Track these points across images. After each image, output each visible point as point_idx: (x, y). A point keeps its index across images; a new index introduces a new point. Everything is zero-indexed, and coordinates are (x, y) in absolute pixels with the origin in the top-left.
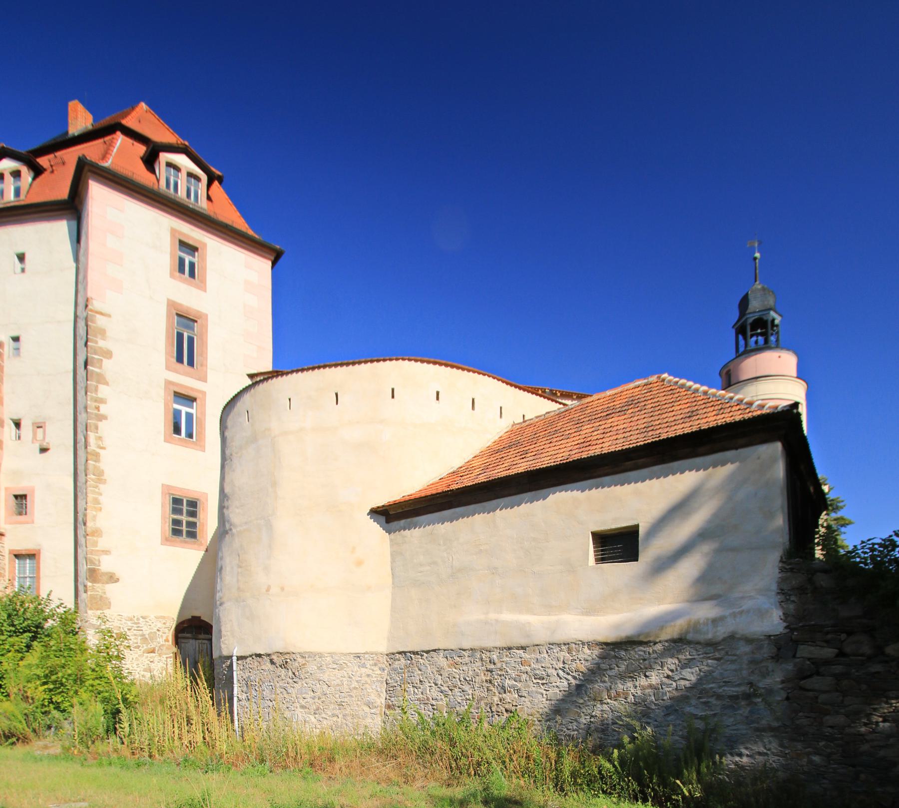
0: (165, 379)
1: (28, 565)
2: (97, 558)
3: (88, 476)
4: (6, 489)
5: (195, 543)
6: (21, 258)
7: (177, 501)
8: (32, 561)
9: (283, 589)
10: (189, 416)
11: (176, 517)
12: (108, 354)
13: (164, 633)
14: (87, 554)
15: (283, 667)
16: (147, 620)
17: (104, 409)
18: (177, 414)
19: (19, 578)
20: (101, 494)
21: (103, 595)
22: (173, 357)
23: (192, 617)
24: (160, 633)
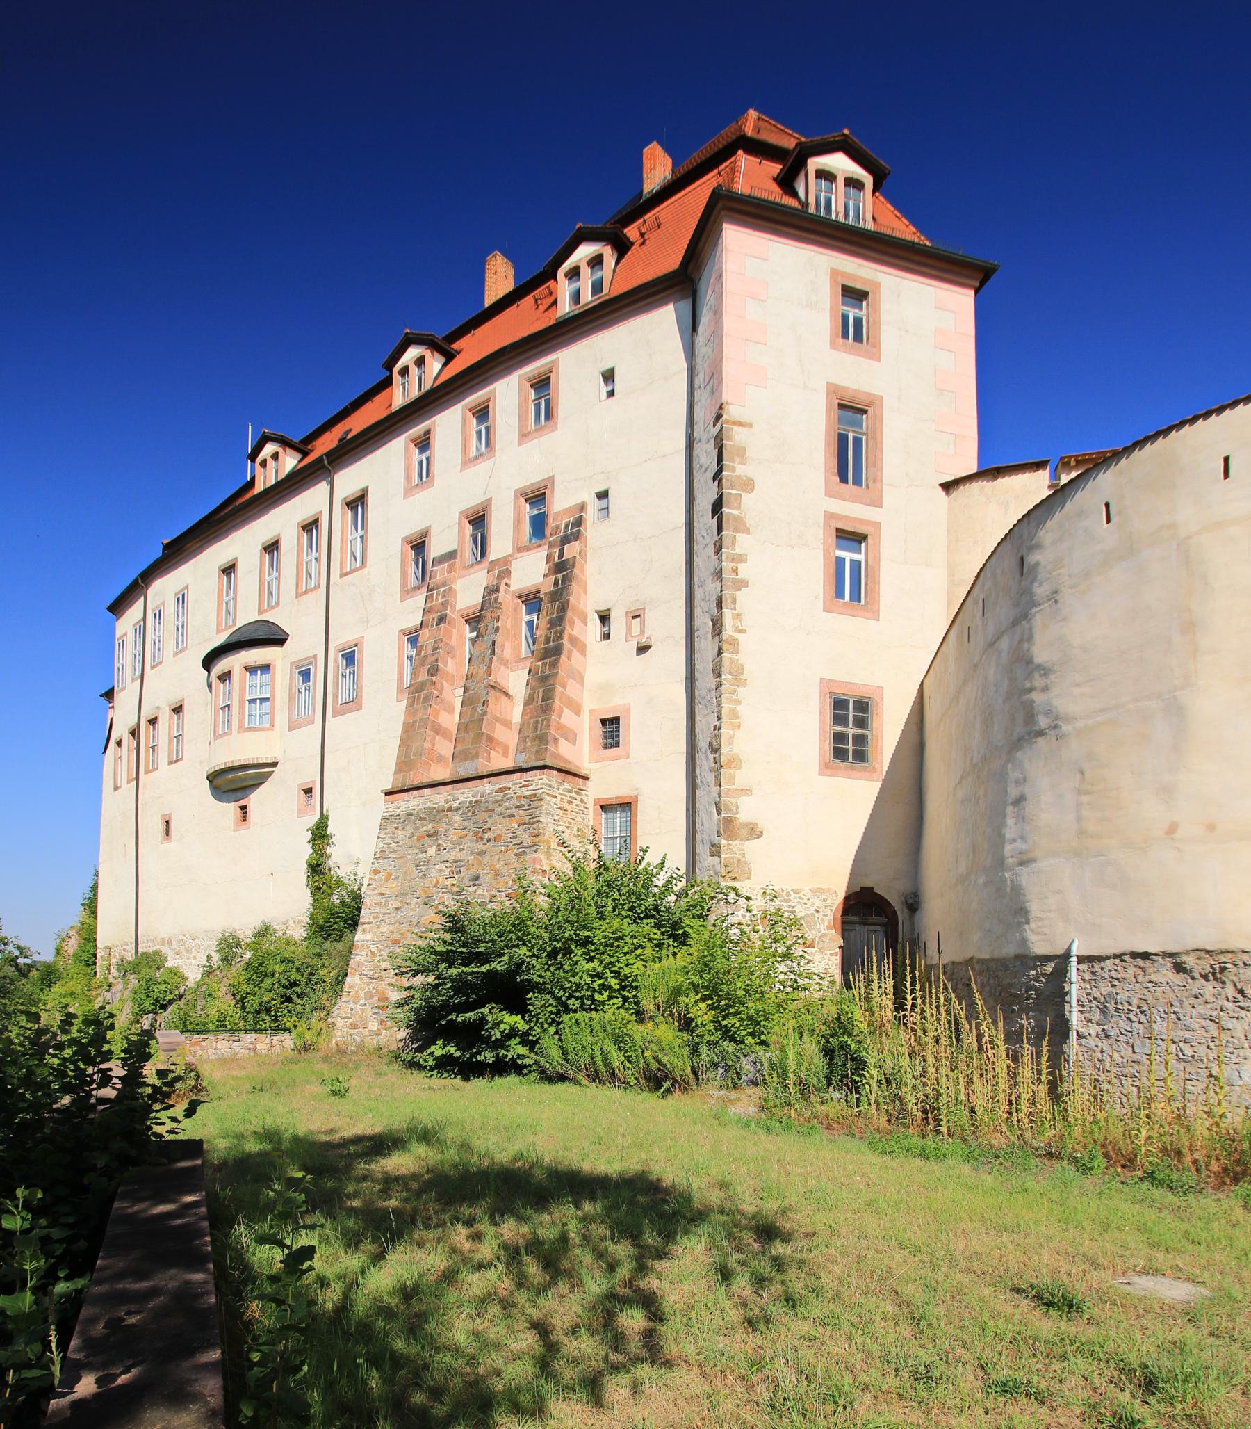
1: (618, 820)
2: (733, 801)
3: (723, 677)
4: (591, 711)
5: (865, 769)
6: (609, 376)
7: (840, 704)
8: (624, 814)
9: (1211, 828)
10: (856, 565)
11: (838, 729)
12: (749, 485)
14: (720, 796)
15: (1211, 977)
16: (801, 895)
17: (744, 571)
19: (607, 838)
20: (739, 703)
21: (741, 857)
24: (820, 915)
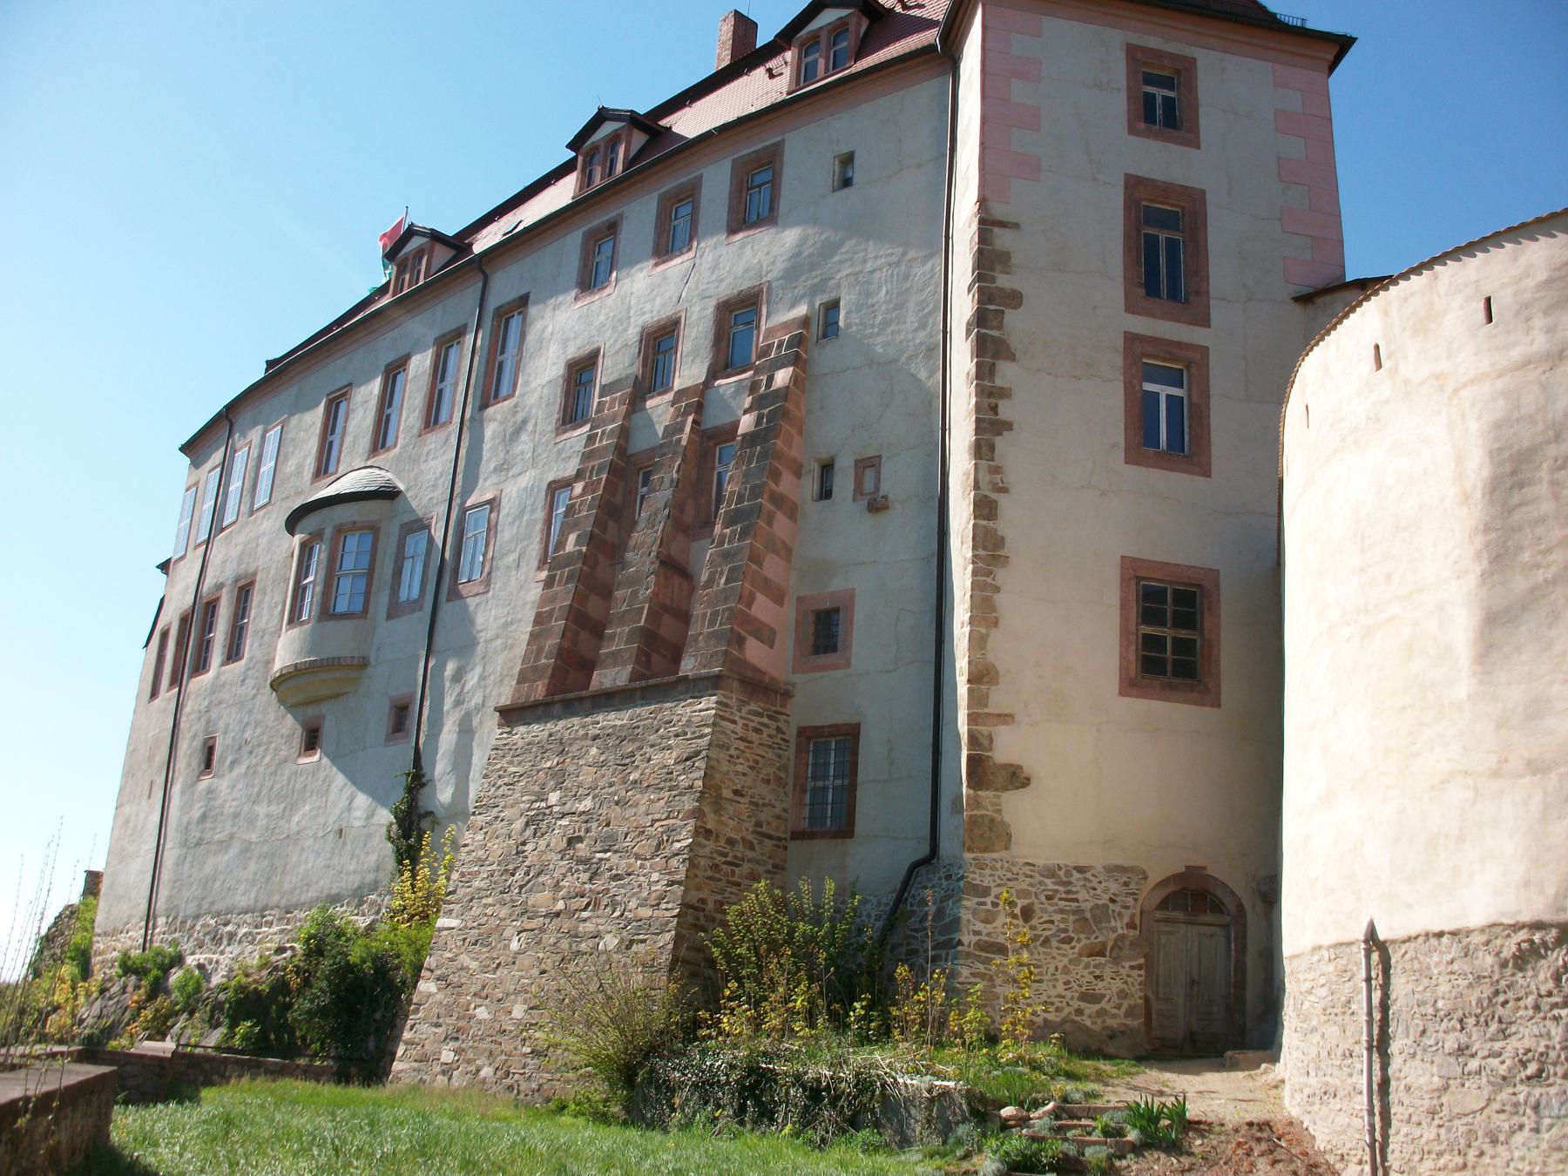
4: (800, 600)
11: (1149, 630)
18: (1151, 242)
20: (997, 589)
23: (1188, 868)
24: (1117, 908)
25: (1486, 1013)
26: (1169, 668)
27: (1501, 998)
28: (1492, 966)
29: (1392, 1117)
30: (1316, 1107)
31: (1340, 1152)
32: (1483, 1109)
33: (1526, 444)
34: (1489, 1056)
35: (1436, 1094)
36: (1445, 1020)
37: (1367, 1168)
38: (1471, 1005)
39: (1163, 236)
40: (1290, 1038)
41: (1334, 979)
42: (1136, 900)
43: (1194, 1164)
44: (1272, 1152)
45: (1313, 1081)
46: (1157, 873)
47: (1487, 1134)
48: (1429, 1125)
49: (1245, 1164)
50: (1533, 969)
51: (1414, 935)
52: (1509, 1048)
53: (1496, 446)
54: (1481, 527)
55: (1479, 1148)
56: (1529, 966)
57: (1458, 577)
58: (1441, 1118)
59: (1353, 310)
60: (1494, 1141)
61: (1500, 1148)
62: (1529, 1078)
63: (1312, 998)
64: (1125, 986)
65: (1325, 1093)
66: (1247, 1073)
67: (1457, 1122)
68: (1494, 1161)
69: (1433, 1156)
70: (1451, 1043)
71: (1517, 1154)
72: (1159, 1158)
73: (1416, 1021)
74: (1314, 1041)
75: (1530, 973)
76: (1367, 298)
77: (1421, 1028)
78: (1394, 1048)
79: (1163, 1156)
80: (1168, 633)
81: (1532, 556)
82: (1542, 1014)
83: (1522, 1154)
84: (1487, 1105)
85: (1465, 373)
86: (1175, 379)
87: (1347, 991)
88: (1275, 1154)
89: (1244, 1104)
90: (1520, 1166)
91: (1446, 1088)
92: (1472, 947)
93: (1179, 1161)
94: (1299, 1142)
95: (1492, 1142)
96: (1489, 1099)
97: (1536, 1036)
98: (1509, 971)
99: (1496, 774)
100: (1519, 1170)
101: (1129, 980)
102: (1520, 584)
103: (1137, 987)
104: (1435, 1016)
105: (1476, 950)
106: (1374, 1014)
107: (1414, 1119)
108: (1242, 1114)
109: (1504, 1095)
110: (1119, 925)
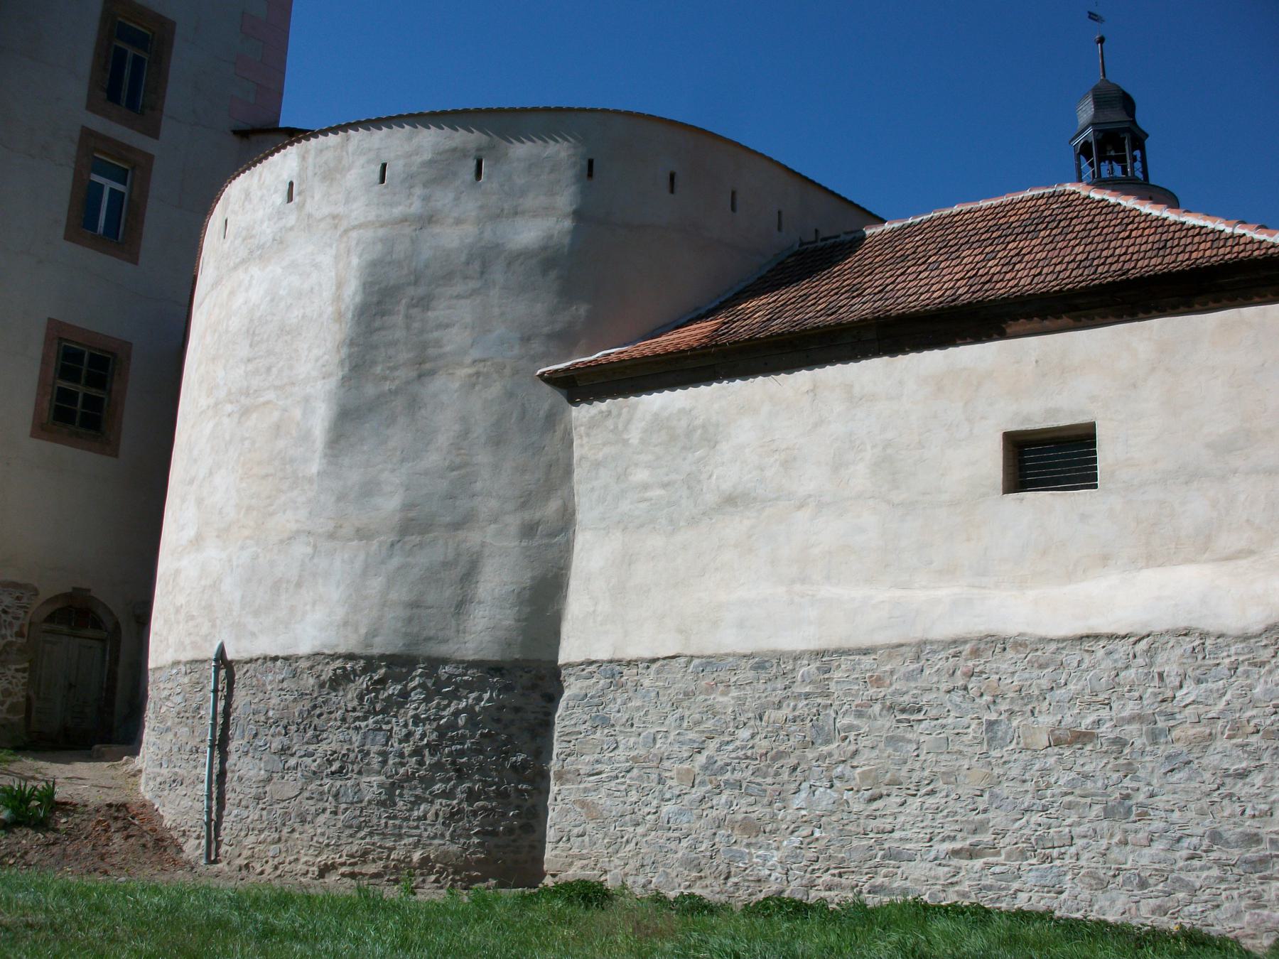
0: (83, 127)
13: (14, 618)
18: (120, 56)
22: (493, 656)
23: (74, 589)
24: (9, 618)
25: (305, 722)
26: (77, 419)
27: (318, 711)
28: (313, 686)
29: (227, 801)
30: (166, 793)
31: (183, 829)
32: (296, 796)
33: (392, 283)
34: (305, 756)
35: (262, 784)
36: (273, 727)
37: (204, 842)
38: (294, 716)
39: (131, 52)
40: (148, 736)
41: (188, 689)
42: (26, 612)
43: (58, 839)
44: (126, 829)
45: (164, 771)
46: (46, 592)
47: (298, 816)
48: (255, 808)
49: (103, 838)
50: (344, 690)
51: (255, 658)
52: (320, 750)
53: (370, 280)
54: (348, 341)
55: (291, 826)
56: (341, 688)
57: (324, 378)
58: (264, 803)
59: (278, 150)
60: (303, 821)
61: (307, 826)
62: (333, 773)
63: (170, 704)
64: (10, 686)
65: (174, 781)
66: (111, 763)
67: (276, 806)
68: (301, 836)
69: (256, 832)
70: (276, 745)
71: (319, 831)
72: (27, 834)
73: (251, 726)
74: (168, 739)
75: (341, 693)
76: (291, 144)
77: (254, 732)
78: (232, 746)
79: (31, 832)
80: (81, 389)
81: (382, 370)
82: (347, 725)
83: (323, 830)
84: (300, 794)
85: (356, 219)
86: (121, 177)
87: (197, 699)
88: (129, 830)
89: (106, 790)
90: (321, 840)
91: (269, 780)
92: (299, 670)
93: (45, 837)
94: (150, 821)
95: (301, 822)
96: (302, 789)
97: (341, 741)
98: (325, 691)
99: (332, 536)
100: (320, 843)
101: (14, 681)
102: (370, 390)
103: (20, 687)
104: (266, 723)
105: (302, 672)
106: (218, 720)
107: (243, 803)
108: (103, 797)
109: (313, 786)
110: (8, 633)
